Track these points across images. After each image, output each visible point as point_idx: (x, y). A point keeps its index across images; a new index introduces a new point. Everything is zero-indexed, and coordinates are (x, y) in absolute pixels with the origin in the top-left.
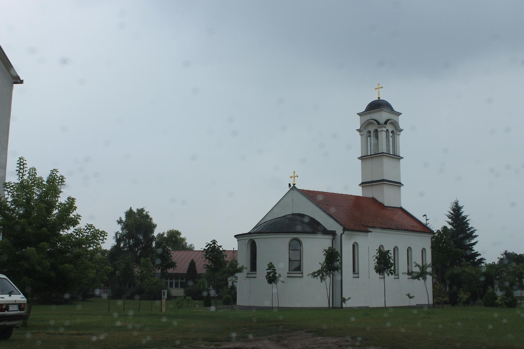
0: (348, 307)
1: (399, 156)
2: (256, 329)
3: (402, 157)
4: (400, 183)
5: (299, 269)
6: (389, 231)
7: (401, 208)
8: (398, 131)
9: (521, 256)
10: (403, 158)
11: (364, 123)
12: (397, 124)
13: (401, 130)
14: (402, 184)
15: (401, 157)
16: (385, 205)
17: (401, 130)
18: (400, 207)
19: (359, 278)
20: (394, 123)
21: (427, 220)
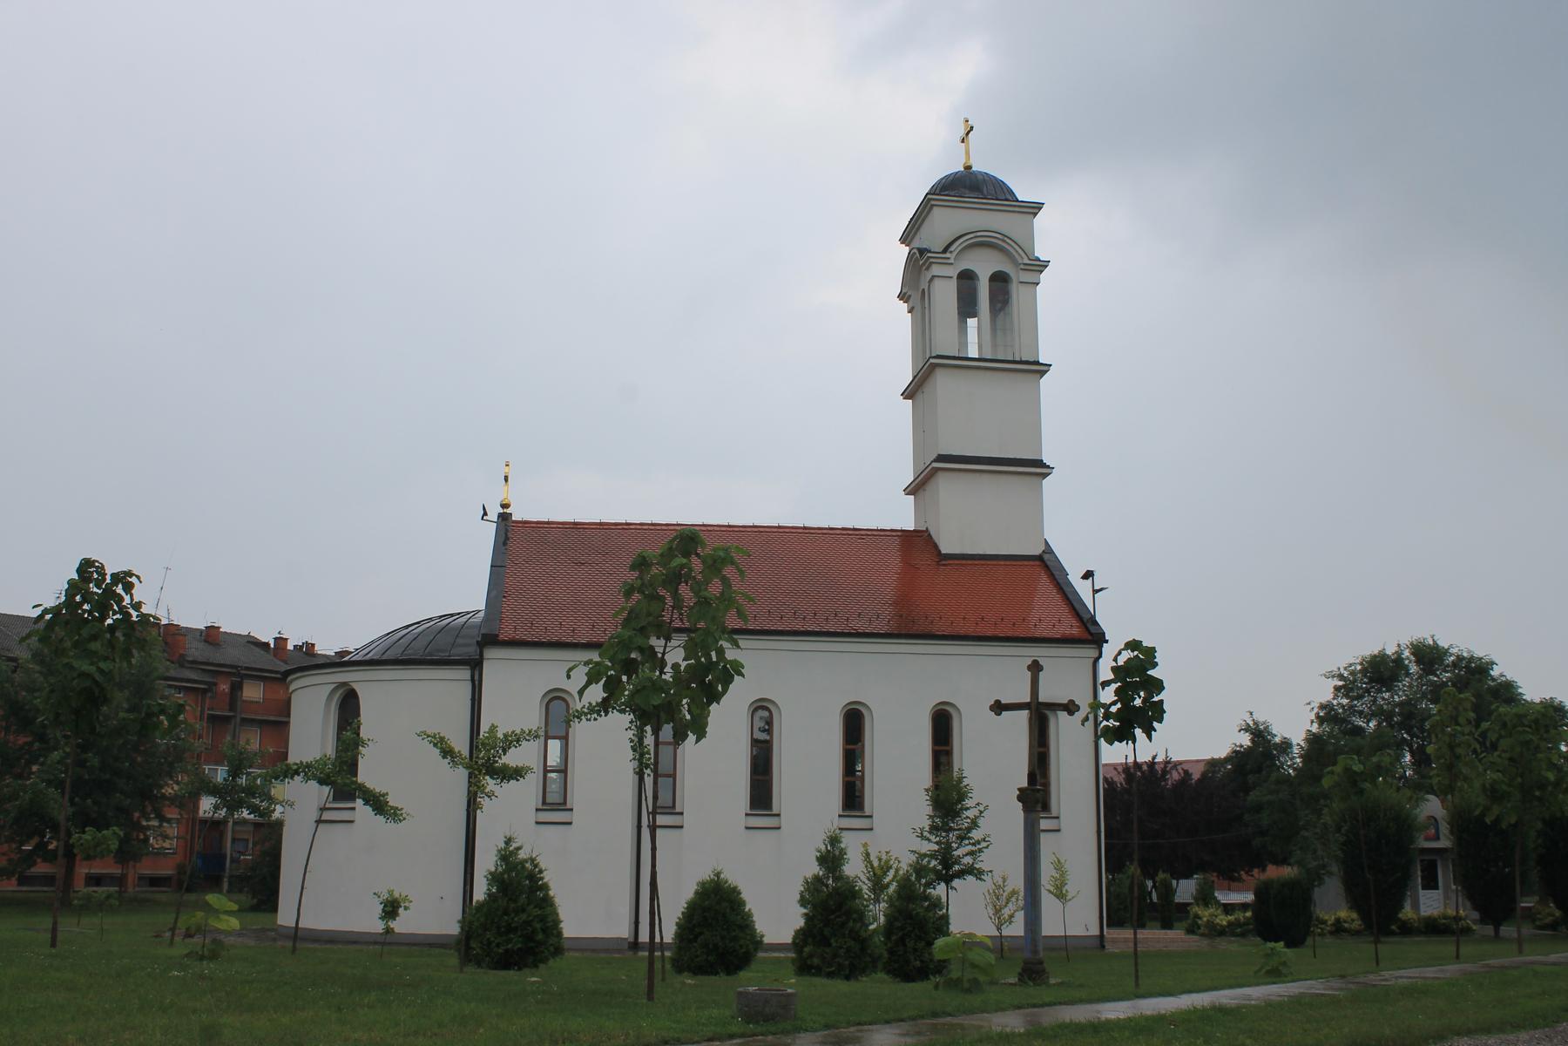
0: (1070, 936)
1: (1037, 363)
2: (935, 1015)
3: (1046, 365)
4: (1040, 463)
5: (562, 805)
6: (328, 676)
7: (1040, 558)
8: (1022, 269)
9: (1551, 713)
10: (1051, 365)
11: (1023, 250)
12: (1008, 244)
13: (1042, 266)
14: (1048, 467)
15: (1042, 364)
16: (943, 552)
17: (1042, 266)
18: (1037, 551)
19: (684, 829)
20: (1000, 242)
21: (1095, 591)
